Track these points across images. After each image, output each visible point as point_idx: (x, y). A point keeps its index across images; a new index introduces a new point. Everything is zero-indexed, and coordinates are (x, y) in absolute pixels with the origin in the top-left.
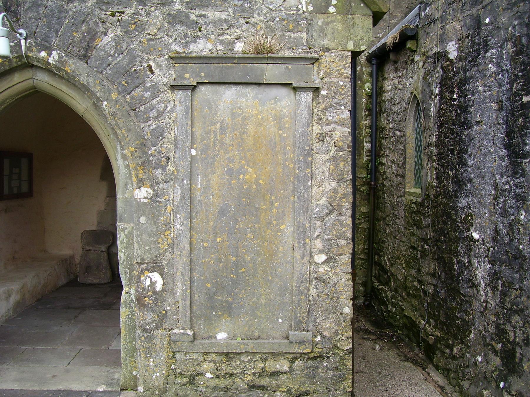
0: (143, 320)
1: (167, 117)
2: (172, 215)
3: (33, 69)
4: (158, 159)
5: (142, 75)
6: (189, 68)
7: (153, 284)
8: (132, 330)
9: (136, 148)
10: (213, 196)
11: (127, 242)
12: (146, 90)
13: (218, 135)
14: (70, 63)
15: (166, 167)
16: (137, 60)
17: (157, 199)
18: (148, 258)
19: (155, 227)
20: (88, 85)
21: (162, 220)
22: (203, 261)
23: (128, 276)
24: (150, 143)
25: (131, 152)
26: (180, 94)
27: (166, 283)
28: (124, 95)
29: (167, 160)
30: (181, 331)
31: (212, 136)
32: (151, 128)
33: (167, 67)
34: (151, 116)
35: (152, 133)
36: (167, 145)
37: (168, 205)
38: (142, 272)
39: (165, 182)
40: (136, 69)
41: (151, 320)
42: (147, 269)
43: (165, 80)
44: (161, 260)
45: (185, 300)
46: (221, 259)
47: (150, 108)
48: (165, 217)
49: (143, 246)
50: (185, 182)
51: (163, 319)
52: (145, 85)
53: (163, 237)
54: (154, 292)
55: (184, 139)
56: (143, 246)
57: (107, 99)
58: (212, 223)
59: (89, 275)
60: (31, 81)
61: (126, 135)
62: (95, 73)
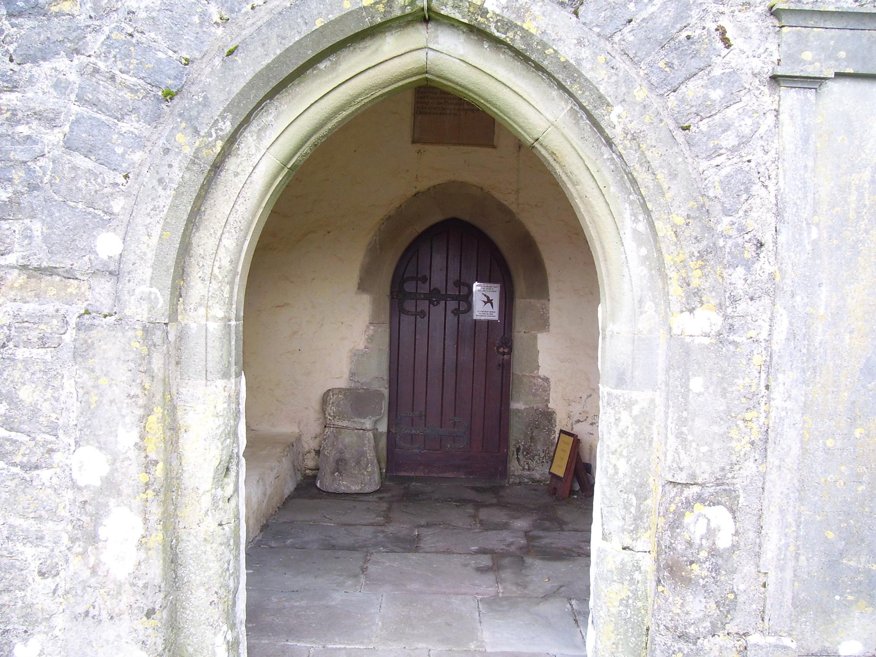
0: (682, 614)
1: (759, 149)
2: (763, 375)
3: (430, 25)
4: (737, 245)
5: (705, 49)
6: (812, 39)
7: (711, 533)
8: (633, 633)
9: (688, 217)
10: (851, 332)
11: (636, 434)
12: (713, 83)
13: (866, 195)
14: (537, 13)
15: (753, 263)
16: (692, 13)
17: (731, 338)
18: (704, 472)
19: (723, 401)
20: (579, 64)
21: (741, 387)
22: (823, 480)
23: (633, 510)
24: (719, 207)
25: (674, 225)
26: (790, 96)
27: (741, 531)
28: (661, 92)
29: (758, 248)
30: (772, 640)
31: (853, 198)
32: (724, 172)
33: (761, 33)
34: (724, 144)
35: (726, 184)
36: (760, 214)
37: (755, 352)
38: (688, 505)
39: (752, 299)
40: (689, 33)
41: (701, 615)
42: (700, 499)
43: (757, 64)
44: (733, 478)
45: (782, 569)
46: (859, 475)
47: (720, 125)
48: (747, 380)
49: (694, 445)
50: (798, 298)
51: (728, 612)
52: (709, 72)
53: (741, 424)
54: (714, 552)
55: (798, 202)
56: (694, 445)
57: (624, 100)
58: (846, 394)
59: (341, 476)
60: (421, 55)
61: (665, 186)
62: (597, 39)
